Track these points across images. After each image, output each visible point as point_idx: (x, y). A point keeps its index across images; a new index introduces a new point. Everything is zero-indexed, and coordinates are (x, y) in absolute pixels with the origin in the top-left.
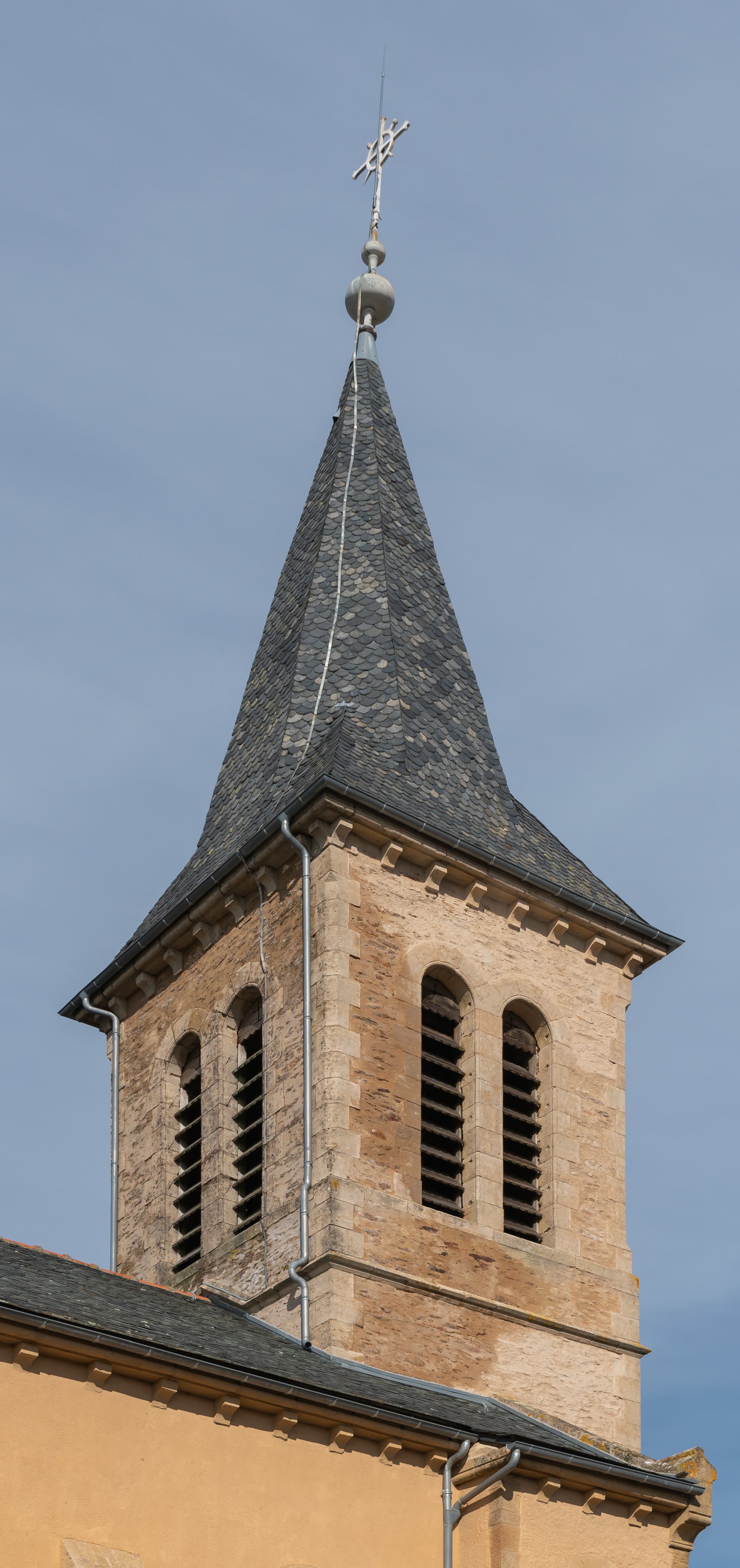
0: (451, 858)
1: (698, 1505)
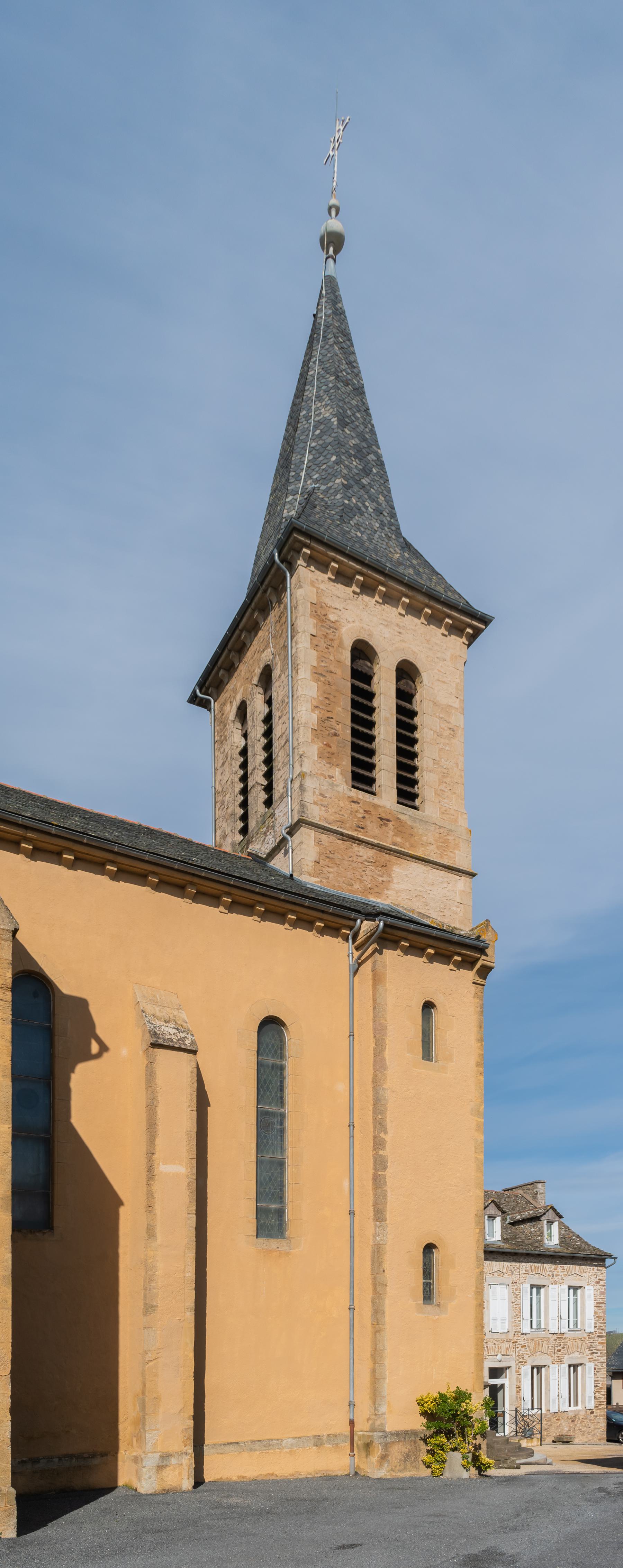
0: (365, 570)
1: (487, 955)
